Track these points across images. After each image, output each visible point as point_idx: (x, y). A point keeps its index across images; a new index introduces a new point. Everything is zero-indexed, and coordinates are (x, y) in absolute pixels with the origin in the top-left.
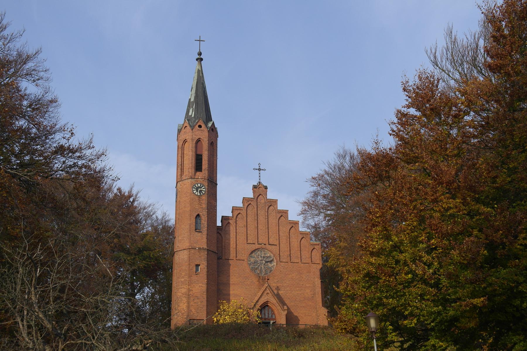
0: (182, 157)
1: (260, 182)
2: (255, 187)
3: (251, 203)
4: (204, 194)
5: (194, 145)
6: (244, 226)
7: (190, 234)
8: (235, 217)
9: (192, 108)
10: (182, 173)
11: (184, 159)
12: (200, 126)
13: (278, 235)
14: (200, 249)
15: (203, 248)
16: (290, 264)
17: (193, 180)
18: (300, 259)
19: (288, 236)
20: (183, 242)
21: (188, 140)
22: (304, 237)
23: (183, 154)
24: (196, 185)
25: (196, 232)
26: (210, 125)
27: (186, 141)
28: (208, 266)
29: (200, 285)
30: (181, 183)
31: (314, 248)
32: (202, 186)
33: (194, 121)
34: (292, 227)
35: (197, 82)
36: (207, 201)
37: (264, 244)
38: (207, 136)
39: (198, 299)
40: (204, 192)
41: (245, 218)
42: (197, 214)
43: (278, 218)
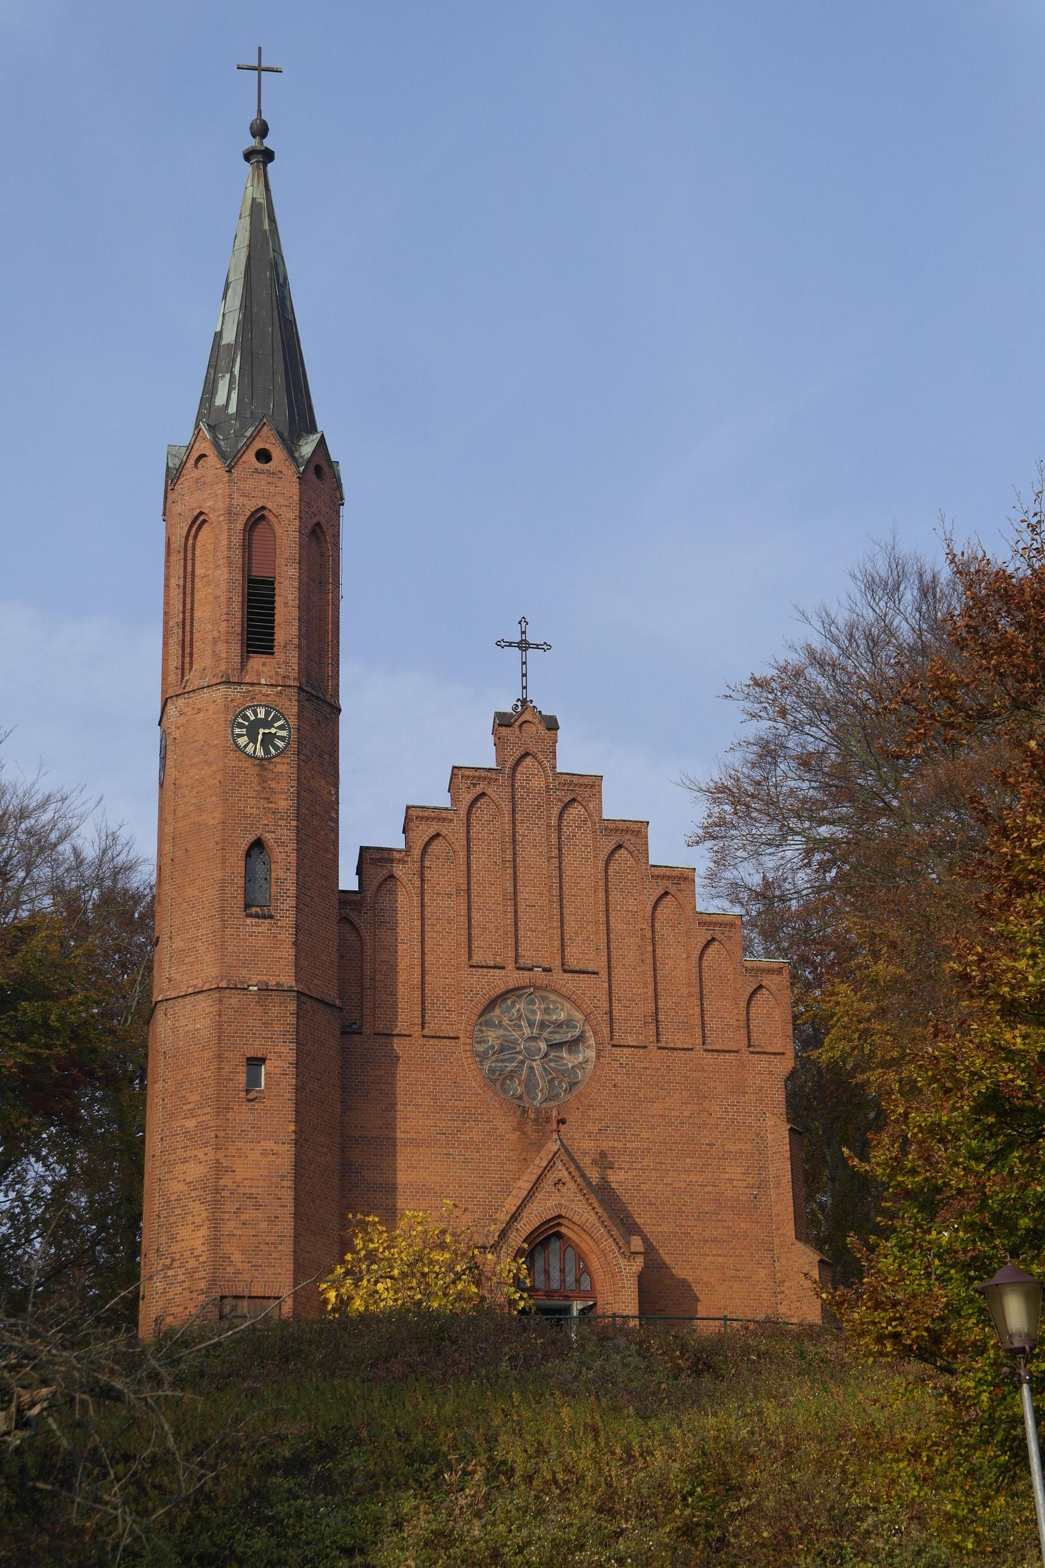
0: (188, 590)
1: (524, 702)
2: (503, 721)
4: (281, 753)
5: (237, 539)
6: (458, 891)
8: (417, 852)
9: (228, 376)
10: (187, 660)
11: (197, 597)
12: (264, 456)
13: (603, 927)
14: (264, 989)
15: (278, 984)
16: (655, 1054)
17: (235, 692)
18: (698, 1034)
19: (649, 934)
20: (191, 959)
21: (212, 517)
22: (719, 936)
23: (189, 577)
24: (249, 713)
26: (307, 448)
27: (204, 521)
28: (302, 1064)
29: (268, 1145)
30: (180, 702)
31: (761, 987)
32: (276, 719)
33: (239, 434)
34: (666, 893)
35: (249, 258)
36: (294, 783)
37: (545, 970)
38: (296, 498)
39: (257, 1206)
40: (281, 744)
41: (462, 854)
42: (251, 838)
43: (603, 855)
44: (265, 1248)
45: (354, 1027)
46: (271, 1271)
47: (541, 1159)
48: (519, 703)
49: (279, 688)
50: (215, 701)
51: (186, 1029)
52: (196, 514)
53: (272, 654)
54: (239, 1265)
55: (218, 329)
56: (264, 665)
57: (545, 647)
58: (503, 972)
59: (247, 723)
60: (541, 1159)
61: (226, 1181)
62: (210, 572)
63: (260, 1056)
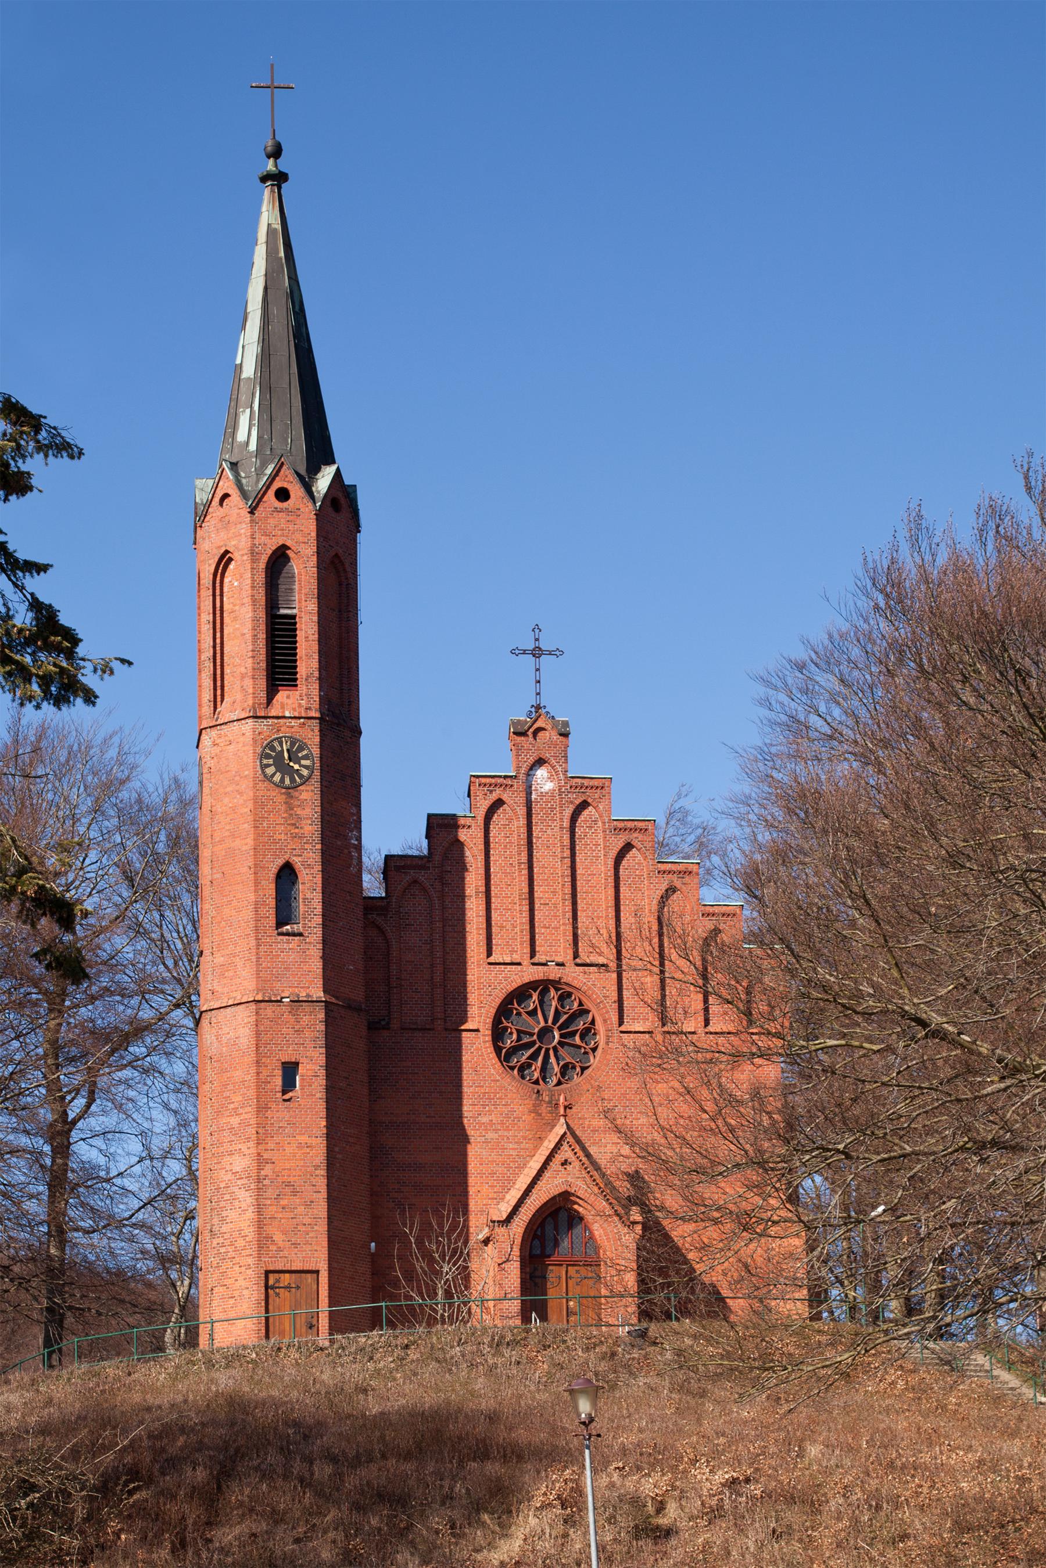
1: (538, 708)
3: (505, 797)
5: (261, 578)
7: (258, 945)
10: (219, 692)
11: (226, 632)
12: (283, 495)
15: (308, 995)
17: (263, 725)
20: (231, 974)
21: (236, 556)
23: (218, 612)
25: (279, 934)
26: (323, 482)
27: (230, 560)
30: (214, 733)
33: (260, 472)
35: (266, 289)
36: (318, 809)
37: (558, 964)
38: (314, 534)
42: (280, 862)
43: (613, 853)
44: (304, 1228)
45: (383, 1023)
46: (309, 1247)
47: (550, 1141)
48: (533, 710)
49: (302, 720)
50: (243, 734)
51: (228, 1036)
52: (222, 551)
53: (296, 686)
54: (281, 1244)
55: (238, 361)
56: (288, 697)
57: (557, 653)
58: (519, 967)
59: (273, 754)
60: (550, 1141)
61: (268, 1170)
62: (237, 608)
63: (293, 1060)
